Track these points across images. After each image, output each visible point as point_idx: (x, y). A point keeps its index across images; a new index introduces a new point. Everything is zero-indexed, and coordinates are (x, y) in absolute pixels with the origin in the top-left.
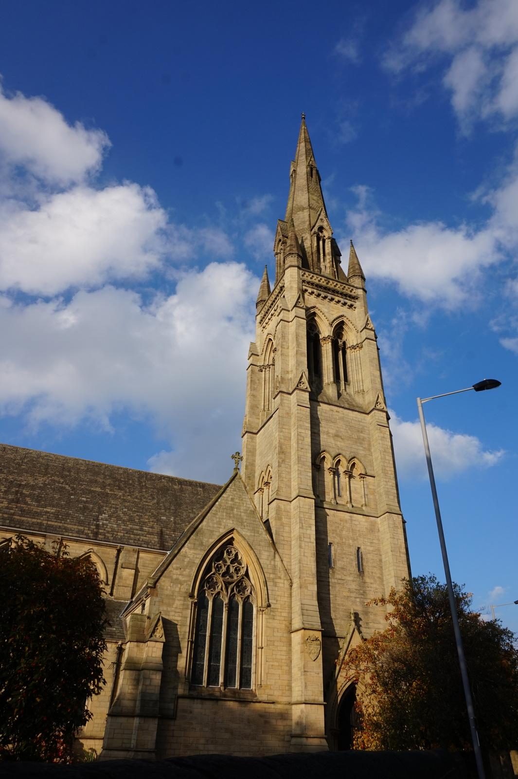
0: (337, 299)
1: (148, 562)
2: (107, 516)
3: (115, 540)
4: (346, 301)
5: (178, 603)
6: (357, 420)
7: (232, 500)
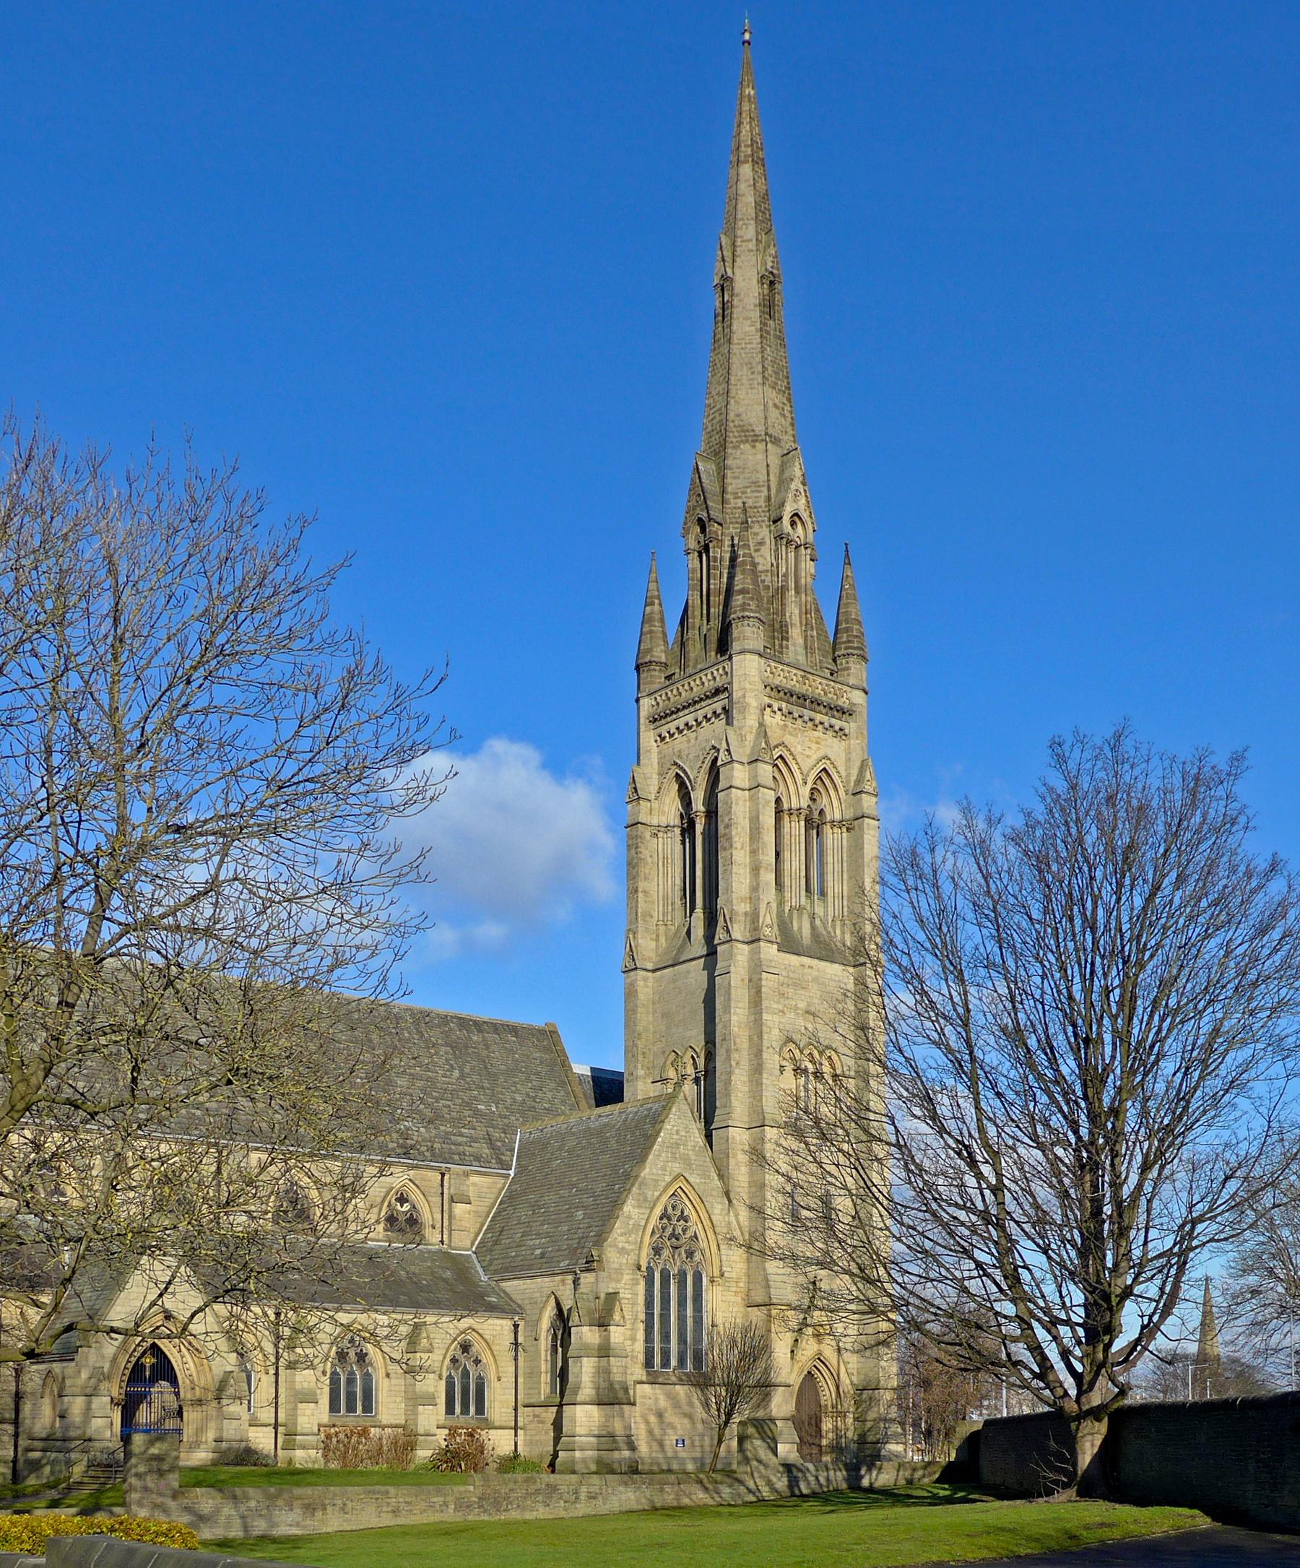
0: (819, 717)
1: (484, 1190)
3: (435, 1157)
4: (833, 721)
5: (627, 1277)
7: (677, 1132)
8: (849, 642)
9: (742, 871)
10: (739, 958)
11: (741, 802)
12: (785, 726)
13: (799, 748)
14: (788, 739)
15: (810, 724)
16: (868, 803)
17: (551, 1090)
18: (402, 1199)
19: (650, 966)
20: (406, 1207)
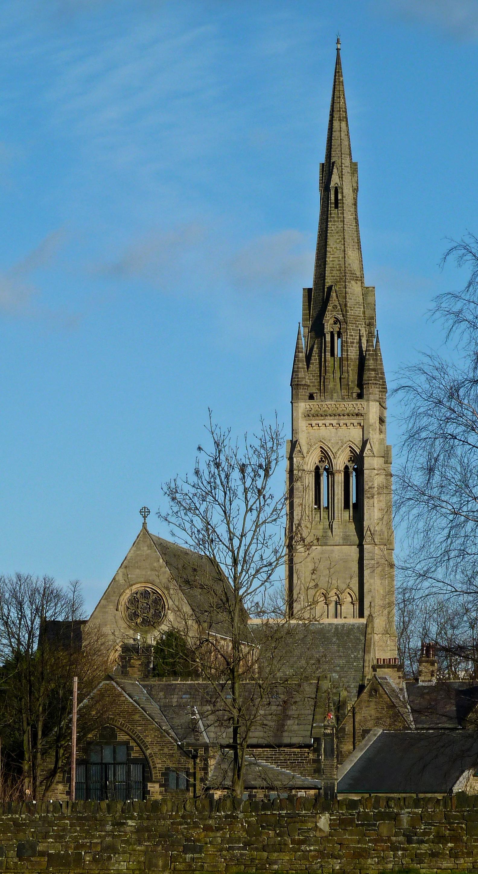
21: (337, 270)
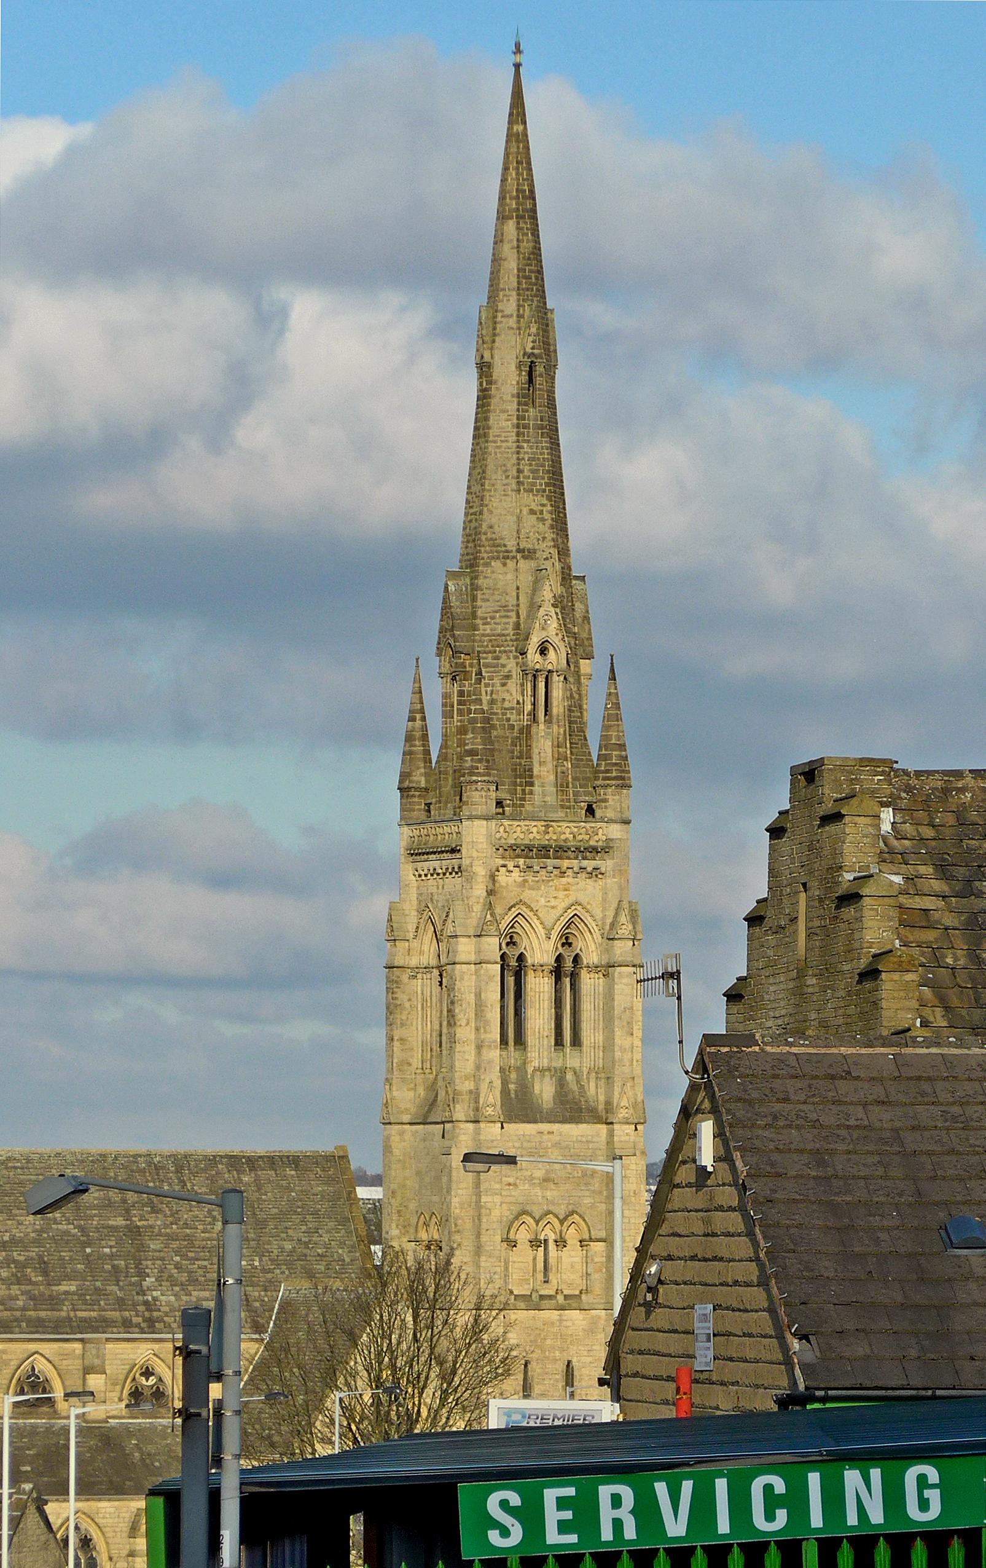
0: (566, 863)
2: (153, 1280)
4: (585, 863)
6: (584, 1139)
8: (607, 771)
9: (467, 1048)
10: (462, 1138)
11: (466, 977)
12: (525, 881)
13: (543, 901)
14: (527, 895)
15: (556, 872)
16: (622, 949)
17: (328, 1232)
18: (147, 1373)
19: (406, 1118)
20: (152, 1380)
21: (496, 714)
